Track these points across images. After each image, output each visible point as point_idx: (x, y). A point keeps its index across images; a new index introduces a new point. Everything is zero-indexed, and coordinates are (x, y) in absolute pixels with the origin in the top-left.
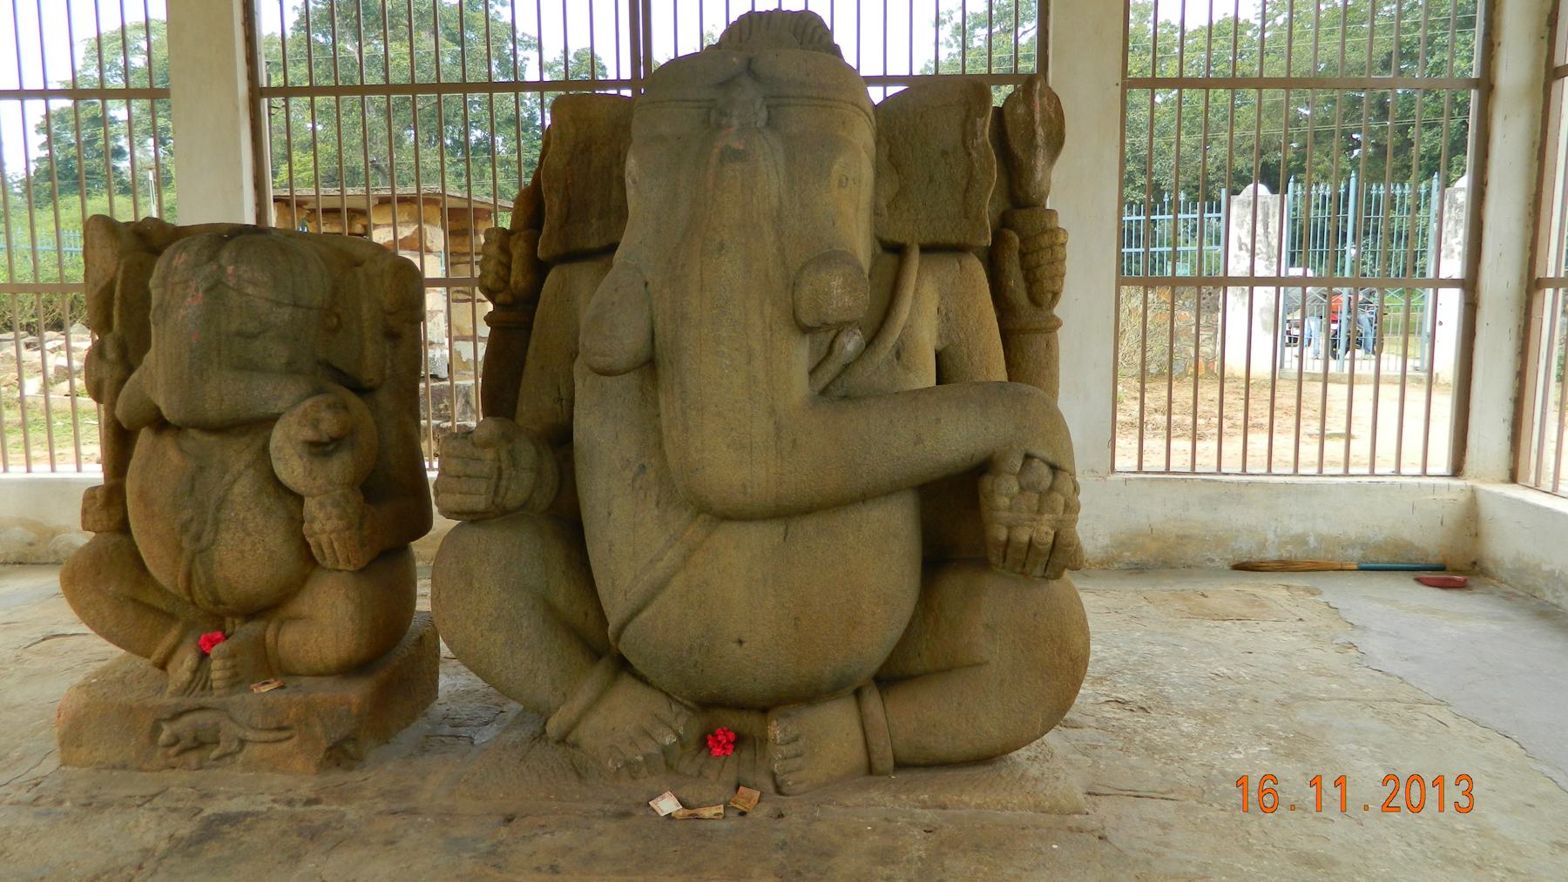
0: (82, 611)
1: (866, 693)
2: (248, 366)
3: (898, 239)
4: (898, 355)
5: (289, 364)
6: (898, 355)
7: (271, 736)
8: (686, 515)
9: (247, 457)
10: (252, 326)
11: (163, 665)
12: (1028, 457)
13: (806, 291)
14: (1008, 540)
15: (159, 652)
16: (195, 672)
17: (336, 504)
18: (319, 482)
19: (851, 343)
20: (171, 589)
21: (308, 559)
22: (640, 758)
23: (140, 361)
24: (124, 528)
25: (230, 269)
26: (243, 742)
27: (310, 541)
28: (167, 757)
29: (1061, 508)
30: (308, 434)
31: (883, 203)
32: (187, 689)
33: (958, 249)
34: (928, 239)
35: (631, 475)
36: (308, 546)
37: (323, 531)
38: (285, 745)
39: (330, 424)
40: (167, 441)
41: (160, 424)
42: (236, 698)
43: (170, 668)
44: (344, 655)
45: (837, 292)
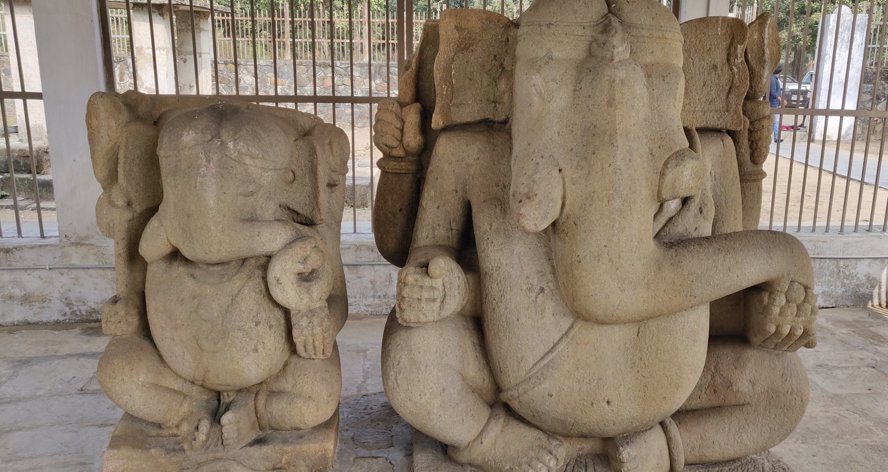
4: (701, 211)
6: (701, 211)
29: (809, 313)
30: (300, 268)
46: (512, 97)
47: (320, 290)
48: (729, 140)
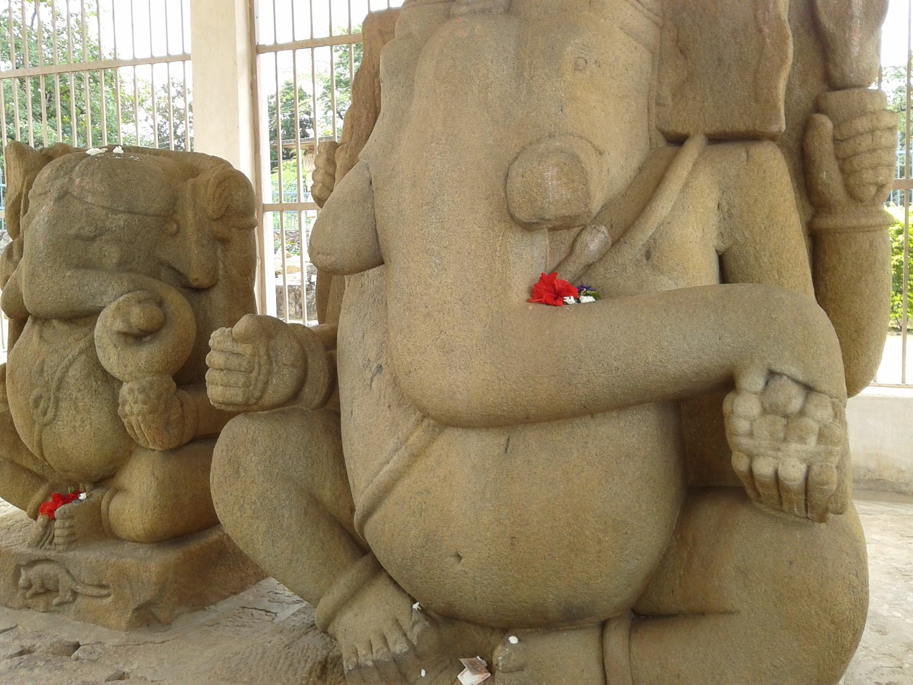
1: (611, 626)
2: (85, 265)
3: (681, 130)
4: (648, 255)
5: (119, 264)
6: (648, 255)
8: (413, 419)
10: (88, 231)
12: (772, 374)
13: (517, 183)
17: (143, 390)
18: (130, 369)
19: (594, 242)
22: (370, 663)
25: (78, 180)
26: (75, 594)
28: (25, 598)
30: (119, 325)
31: (666, 93)
33: (750, 138)
34: (714, 127)
35: (371, 375)
37: (132, 413)
39: (138, 317)
42: (71, 554)
44: (147, 526)
45: (552, 184)
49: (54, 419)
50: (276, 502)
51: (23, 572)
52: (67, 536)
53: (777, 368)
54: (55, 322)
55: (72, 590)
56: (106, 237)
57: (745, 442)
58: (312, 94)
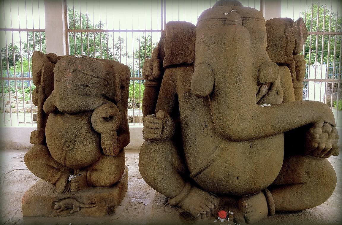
0: (30, 168)
4: (277, 93)
6: (277, 93)
7: (89, 206)
9: (84, 122)
10: (86, 83)
11: (54, 184)
12: (325, 122)
13: (262, 73)
14: (318, 147)
15: (54, 180)
16: (66, 187)
18: (106, 130)
20: (58, 161)
21: (101, 152)
23: (50, 93)
24: (44, 143)
25: (79, 66)
26: (80, 208)
27: (103, 147)
30: (104, 115)
32: (64, 192)
36: (102, 149)
38: (94, 209)
39: (110, 112)
40: (59, 118)
41: (56, 112)
43: (57, 185)
44: (112, 181)
46: (194, 53)
47: (112, 125)
48: (287, 68)
49: (73, 148)
50: (165, 168)
51: (56, 203)
52: (77, 188)
53: (326, 121)
54: (67, 115)
55: (79, 207)
56: (91, 85)
57: (318, 140)
58: (20, 47)
